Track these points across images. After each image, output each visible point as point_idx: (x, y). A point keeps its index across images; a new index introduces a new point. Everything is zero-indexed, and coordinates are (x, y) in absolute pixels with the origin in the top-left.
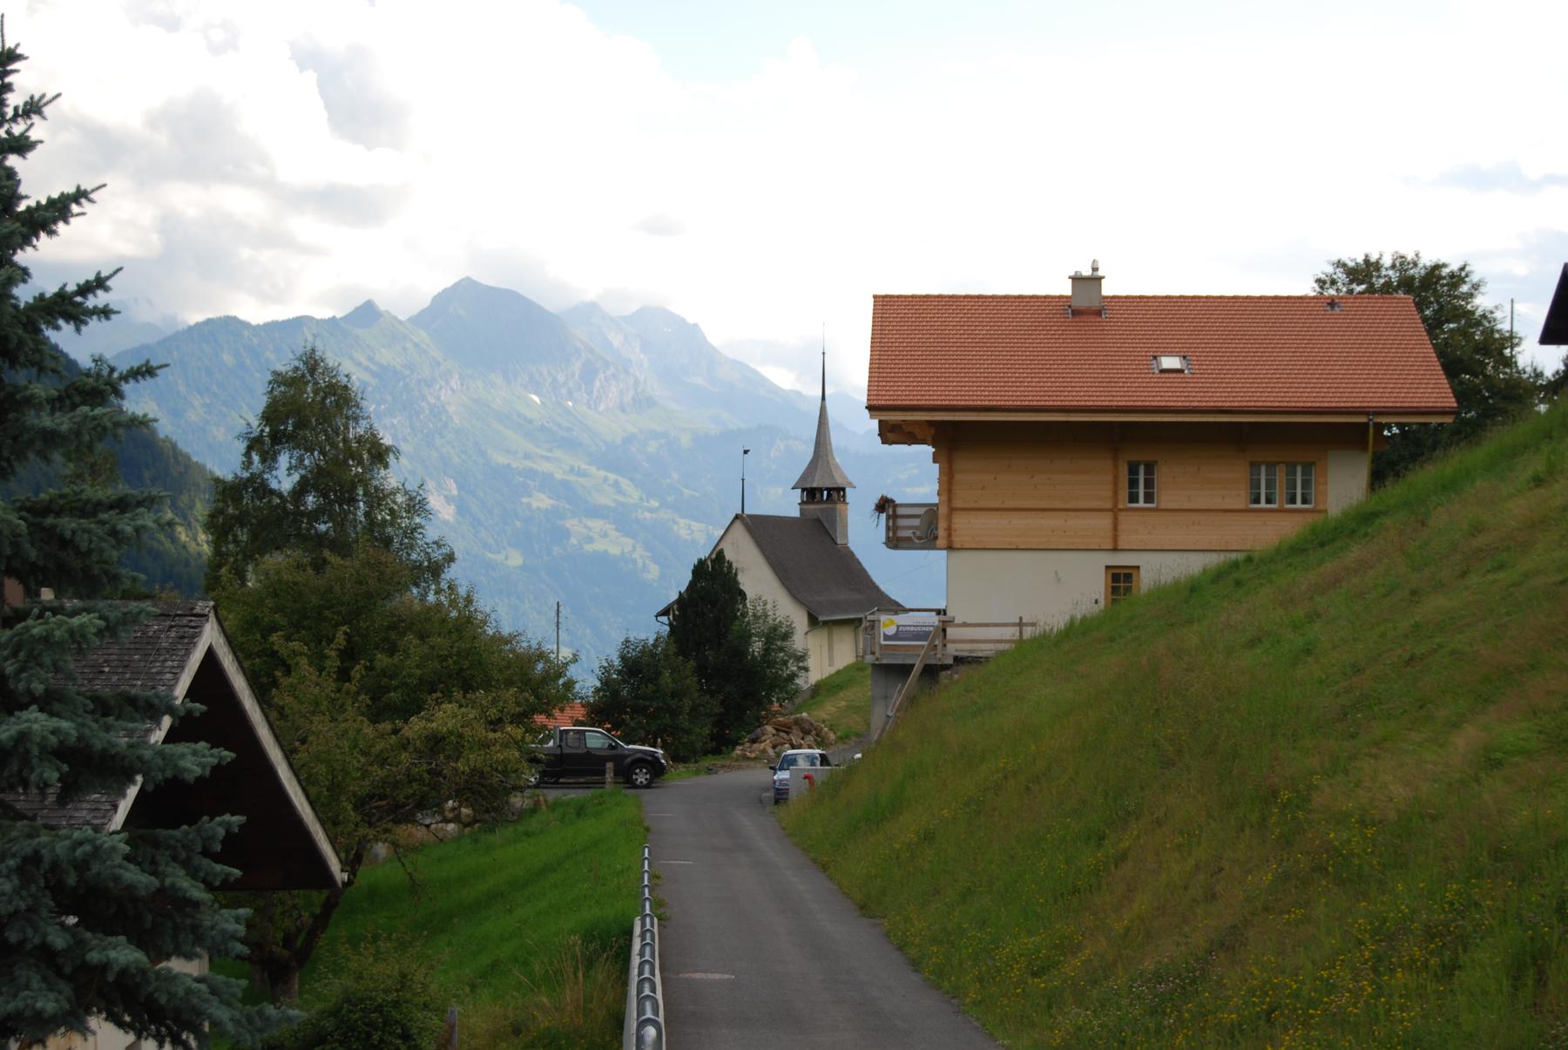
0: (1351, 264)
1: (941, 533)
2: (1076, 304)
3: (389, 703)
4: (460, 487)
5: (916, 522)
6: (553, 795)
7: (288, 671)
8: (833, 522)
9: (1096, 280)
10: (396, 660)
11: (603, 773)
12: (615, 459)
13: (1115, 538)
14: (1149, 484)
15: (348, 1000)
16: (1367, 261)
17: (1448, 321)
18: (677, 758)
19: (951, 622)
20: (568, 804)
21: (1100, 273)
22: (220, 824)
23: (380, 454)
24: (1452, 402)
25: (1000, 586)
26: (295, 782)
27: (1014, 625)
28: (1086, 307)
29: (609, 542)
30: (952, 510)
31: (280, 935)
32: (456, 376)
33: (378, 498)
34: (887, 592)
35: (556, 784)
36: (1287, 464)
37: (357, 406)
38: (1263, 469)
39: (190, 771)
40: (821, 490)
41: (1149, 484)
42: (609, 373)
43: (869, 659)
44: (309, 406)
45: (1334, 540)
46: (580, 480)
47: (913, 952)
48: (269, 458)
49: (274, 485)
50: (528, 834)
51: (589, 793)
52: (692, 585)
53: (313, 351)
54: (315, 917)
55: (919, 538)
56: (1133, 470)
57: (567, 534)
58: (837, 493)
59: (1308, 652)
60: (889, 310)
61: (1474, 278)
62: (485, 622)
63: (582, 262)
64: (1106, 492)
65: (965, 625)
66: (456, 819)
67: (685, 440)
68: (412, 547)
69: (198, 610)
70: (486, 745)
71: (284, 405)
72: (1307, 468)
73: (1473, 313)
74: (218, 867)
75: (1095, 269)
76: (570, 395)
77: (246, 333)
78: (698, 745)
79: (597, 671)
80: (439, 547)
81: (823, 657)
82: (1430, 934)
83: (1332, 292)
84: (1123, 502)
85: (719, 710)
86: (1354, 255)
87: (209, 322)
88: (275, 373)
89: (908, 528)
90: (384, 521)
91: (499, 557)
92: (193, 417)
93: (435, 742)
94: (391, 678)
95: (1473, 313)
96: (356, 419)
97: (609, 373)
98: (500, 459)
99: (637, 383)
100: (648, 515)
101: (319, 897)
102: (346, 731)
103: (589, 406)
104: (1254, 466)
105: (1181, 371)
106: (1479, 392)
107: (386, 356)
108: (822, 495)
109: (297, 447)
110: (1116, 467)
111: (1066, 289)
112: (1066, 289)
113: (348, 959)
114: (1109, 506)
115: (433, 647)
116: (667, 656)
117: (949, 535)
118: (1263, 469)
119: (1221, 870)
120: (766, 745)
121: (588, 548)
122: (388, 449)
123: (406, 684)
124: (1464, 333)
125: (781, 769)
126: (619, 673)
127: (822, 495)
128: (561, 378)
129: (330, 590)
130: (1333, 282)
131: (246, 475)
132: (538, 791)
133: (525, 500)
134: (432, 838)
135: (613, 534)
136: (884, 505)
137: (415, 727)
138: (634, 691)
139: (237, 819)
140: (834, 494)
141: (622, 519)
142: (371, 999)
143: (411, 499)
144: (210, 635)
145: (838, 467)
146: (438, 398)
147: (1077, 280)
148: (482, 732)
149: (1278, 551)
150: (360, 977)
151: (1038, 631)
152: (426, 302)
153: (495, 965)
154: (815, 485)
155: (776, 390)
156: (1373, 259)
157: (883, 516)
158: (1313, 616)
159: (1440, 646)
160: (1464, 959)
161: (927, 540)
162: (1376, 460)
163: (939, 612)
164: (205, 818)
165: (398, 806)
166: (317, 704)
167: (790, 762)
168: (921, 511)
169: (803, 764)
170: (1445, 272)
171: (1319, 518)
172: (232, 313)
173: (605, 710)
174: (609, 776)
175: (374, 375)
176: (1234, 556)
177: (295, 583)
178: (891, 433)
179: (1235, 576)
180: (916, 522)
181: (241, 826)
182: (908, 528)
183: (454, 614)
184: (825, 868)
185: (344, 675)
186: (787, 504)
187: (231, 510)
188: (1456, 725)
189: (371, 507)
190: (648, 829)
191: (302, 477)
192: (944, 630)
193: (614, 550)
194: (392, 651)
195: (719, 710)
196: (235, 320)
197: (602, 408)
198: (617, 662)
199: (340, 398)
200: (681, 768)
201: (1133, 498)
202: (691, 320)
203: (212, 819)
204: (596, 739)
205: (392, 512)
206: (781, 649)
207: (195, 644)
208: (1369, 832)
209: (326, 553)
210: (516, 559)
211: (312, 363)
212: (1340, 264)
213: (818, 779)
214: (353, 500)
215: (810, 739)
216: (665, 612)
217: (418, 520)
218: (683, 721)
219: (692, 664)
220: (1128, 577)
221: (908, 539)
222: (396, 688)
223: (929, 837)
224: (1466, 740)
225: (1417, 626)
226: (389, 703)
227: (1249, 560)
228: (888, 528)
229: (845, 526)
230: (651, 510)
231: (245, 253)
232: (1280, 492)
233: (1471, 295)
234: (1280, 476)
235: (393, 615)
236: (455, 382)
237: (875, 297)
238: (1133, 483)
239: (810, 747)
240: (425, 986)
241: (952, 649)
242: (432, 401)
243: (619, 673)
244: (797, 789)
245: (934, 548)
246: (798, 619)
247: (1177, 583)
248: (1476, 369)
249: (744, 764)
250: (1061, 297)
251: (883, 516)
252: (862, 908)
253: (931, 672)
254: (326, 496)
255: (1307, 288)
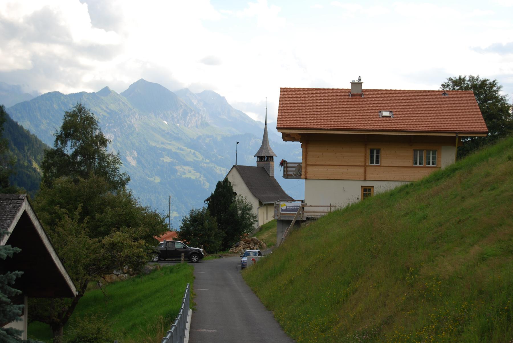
0: (454, 79)
1: (303, 173)
2: (354, 92)
3: (96, 232)
4: (138, 154)
5: (294, 169)
6: (162, 265)
7: (60, 219)
8: (269, 169)
9: (360, 84)
10: (103, 216)
11: (180, 257)
12: (194, 145)
13: (365, 176)
14: (377, 157)
15: (79, 337)
16: (460, 78)
17: (489, 100)
18: (209, 252)
19: (306, 205)
20: (167, 268)
21: (362, 81)
22: (14, 274)
23: (104, 142)
24: (486, 129)
25: (323, 193)
26: (58, 259)
27: (328, 206)
28: (356, 93)
29: (191, 174)
30: (307, 165)
31: (56, 314)
32: (137, 114)
33: (103, 158)
34: (287, 194)
35: (164, 261)
36: (427, 150)
37: (96, 124)
38: (418, 152)
39: (3, 255)
40: (264, 157)
41: (377, 157)
42: (192, 114)
43: (276, 218)
44: (79, 124)
45: (442, 178)
46: (181, 152)
47: (282, 323)
48: (64, 143)
49: (66, 152)
50: (152, 279)
51: (175, 264)
52: (216, 191)
53: (80, 105)
54: (69, 307)
55: (295, 175)
56: (372, 152)
57: (176, 171)
58: (270, 158)
59: (424, 218)
60: (285, 92)
61: (498, 85)
62: (135, 203)
63: (184, 74)
64: (363, 160)
65: (311, 206)
66: (128, 273)
67: (219, 138)
68: (114, 175)
69: (20, 197)
70: (131, 247)
71: (70, 124)
72: (434, 152)
73: (498, 97)
74: (13, 290)
75: (360, 80)
76: (178, 122)
77: (62, 98)
78: (217, 248)
79: (181, 221)
80: (125, 175)
81: (263, 217)
82: (455, 320)
83: (448, 89)
84: (368, 163)
85: (225, 235)
86: (456, 76)
87: (49, 93)
88: (67, 112)
89: (293, 172)
90: (105, 165)
91: (152, 179)
92: (43, 127)
93: (113, 246)
94: (101, 222)
95: (498, 97)
96: (95, 129)
97: (192, 114)
98: (153, 144)
99: (202, 117)
100: (205, 165)
101: (70, 300)
102: (81, 241)
103: (185, 126)
104: (415, 151)
105: (389, 117)
106: (500, 125)
107: (112, 107)
108: (265, 158)
109: (74, 139)
110: (366, 151)
111: (349, 87)
112: (349, 87)
113: (80, 323)
114: (363, 164)
115: (116, 212)
116: (206, 216)
117: (306, 174)
118: (418, 152)
119: (388, 296)
120: (241, 248)
121: (184, 176)
122: (107, 140)
123: (106, 225)
124: (494, 104)
125: (244, 257)
126: (190, 221)
127: (265, 158)
128: (175, 115)
129: (80, 190)
130: (448, 86)
131: (56, 148)
132: (156, 263)
133: (161, 159)
134: (119, 280)
135: (193, 171)
136: (283, 163)
137: (107, 240)
138: (195, 229)
139: (20, 273)
140: (269, 159)
141: (196, 166)
142: (87, 337)
143: (115, 158)
144: (25, 206)
145: (271, 149)
146: (131, 122)
147: (353, 83)
148: (130, 242)
149: (422, 182)
150: (83, 329)
151: (336, 209)
152: (127, 87)
153: (134, 326)
154: (262, 155)
155: (252, 121)
156: (462, 77)
157: (283, 167)
158: (428, 205)
159: (470, 217)
160: (465, 330)
161: (298, 175)
162: (459, 150)
163: (302, 201)
164: (9, 272)
165: (100, 268)
166: (71, 231)
167: (248, 254)
168: (296, 165)
169: (252, 255)
170: (488, 82)
171: (437, 170)
172: (57, 90)
173: (185, 234)
174: (182, 258)
175: (108, 113)
176: (406, 183)
177: (67, 188)
178: (286, 137)
179: (405, 191)
180: (294, 169)
181: (22, 275)
182: (293, 172)
183: (124, 200)
184: (255, 292)
185: (81, 221)
186: (252, 161)
187: (50, 161)
188: (472, 245)
189: (100, 161)
190: (194, 278)
191: (76, 150)
192: (303, 208)
193: (193, 177)
194: (102, 213)
195: (225, 235)
196: (58, 92)
197: (189, 126)
198: (189, 217)
199: (90, 122)
200: (210, 256)
201: (372, 162)
202: (222, 96)
203: (11, 273)
204: (179, 245)
205: (108, 162)
206: (248, 214)
207: (19, 210)
208: (439, 283)
209: (79, 177)
210: (158, 180)
211: (80, 109)
212: (450, 79)
213: (257, 260)
214: (94, 158)
215: (257, 246)
216: (207, 200)
217: (117, 166)
218: (212, 239)
219: (216, 218)
220: (370, 190)
221: (291, 175)
222: (103, 226)
223: (292, 282)
224: (475, 250)
225: (463, 210)
226: (96, 232)
227: (412, 184)
228: (284, 171)
229: (273, 170)
230: (207, 163)
231: (61, 69)
232: (424, 161)
233: (497, 91)
234: (425, 155)
235: (102, 200)
236: (137, 116)
237: (281, 88)
238: (372, 157)
239: (257, 249)
240: (107, 333)
241: (306, 215)
242: (129, 123)
243: (190, 221)
244: (249, 264)
245: (301, 179)
246: (254, 203)
247: (386, 192)
248: (499, 118)
249: (233, 255)
250: (347, 89)
251: (283, 167)
252: (267, 307)
253: (298, 223)
254: (84, 157)
255: (437, 87)
